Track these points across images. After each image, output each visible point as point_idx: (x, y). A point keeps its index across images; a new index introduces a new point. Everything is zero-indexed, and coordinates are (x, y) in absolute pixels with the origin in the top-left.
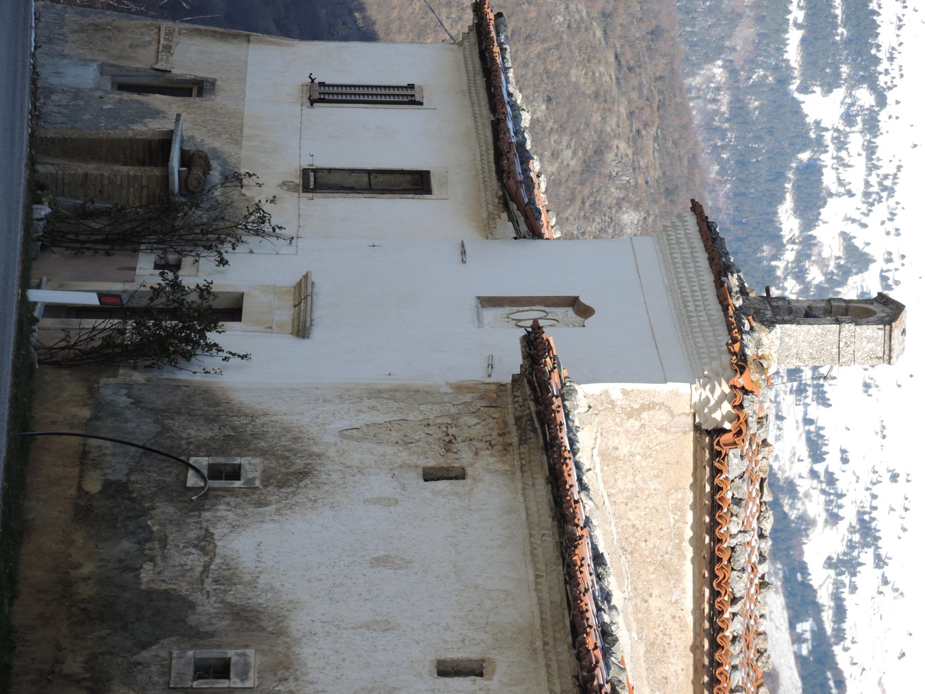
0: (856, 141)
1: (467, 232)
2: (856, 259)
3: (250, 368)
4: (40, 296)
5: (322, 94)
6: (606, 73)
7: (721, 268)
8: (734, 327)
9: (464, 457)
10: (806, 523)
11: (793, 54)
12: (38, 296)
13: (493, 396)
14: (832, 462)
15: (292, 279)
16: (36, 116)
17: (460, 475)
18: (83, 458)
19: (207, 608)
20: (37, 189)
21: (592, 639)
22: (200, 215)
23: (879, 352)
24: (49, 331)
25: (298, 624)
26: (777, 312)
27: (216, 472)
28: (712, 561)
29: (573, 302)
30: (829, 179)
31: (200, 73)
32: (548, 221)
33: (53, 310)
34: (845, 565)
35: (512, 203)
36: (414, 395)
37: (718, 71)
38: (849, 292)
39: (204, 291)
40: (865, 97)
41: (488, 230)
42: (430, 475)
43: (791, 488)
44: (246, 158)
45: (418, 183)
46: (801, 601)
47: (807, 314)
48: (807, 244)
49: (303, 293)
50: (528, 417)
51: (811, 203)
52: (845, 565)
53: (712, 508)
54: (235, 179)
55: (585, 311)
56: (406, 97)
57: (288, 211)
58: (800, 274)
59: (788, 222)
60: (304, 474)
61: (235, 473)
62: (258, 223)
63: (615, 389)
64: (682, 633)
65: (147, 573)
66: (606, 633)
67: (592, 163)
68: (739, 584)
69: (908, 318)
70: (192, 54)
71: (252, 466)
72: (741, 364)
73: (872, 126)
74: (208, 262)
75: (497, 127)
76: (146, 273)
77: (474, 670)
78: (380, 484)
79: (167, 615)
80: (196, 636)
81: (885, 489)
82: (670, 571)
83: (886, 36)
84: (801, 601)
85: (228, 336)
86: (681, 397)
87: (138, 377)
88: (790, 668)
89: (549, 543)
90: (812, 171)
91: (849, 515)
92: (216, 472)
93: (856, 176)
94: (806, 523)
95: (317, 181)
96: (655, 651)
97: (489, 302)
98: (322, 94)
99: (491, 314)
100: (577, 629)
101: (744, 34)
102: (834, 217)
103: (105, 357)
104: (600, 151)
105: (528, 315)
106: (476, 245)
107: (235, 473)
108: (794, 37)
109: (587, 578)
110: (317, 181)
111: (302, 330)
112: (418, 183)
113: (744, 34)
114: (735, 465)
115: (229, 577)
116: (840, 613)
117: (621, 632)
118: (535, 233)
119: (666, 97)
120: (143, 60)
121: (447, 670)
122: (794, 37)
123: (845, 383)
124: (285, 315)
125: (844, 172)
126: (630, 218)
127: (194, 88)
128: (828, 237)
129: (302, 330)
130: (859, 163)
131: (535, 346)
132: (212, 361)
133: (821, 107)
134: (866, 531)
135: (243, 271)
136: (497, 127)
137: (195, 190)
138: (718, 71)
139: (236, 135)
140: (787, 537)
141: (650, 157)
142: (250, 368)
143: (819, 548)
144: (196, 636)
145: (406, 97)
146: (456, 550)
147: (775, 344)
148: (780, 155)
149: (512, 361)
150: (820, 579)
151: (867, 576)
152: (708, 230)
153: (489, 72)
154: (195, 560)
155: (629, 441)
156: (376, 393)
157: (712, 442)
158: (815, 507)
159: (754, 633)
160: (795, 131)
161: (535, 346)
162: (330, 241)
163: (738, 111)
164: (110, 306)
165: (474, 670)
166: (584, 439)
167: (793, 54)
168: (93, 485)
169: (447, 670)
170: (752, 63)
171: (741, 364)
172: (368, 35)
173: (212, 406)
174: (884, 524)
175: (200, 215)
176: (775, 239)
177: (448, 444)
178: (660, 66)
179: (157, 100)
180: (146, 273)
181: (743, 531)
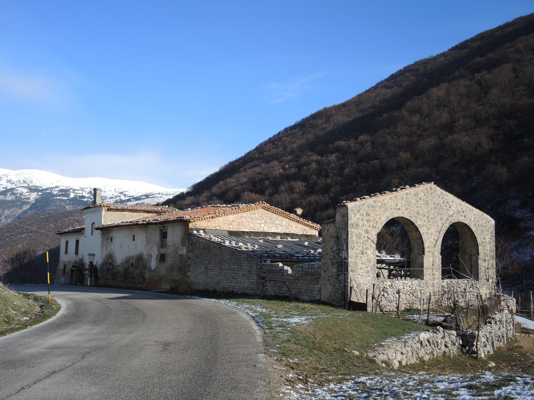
0: (76, 192)
1: (84, 236)
2: (90, 192)
3: (98, 260)
4: (89, 284)
5: (66, 252)
6: (67, 219)
7: (89, 208)
8: (96, 207)
9: (110, 237)
10: (120, 199)
11: (66, 198)
12: (89, 284)
13: (103, 234)
14: (113, 196)
15: (88, 256)
16: (68, 284)
17: (112, 238)
18: (108, 279)
19: (126, 266)
20: (76, 284)
21: (131, 224)
22: (80, 266)
23: (97, 192)
24: (93, 283)
25: (128, 256)
26: (94, 202)
27: (110, 265)
28: (123, 210)
29: (92, 224)
30: (80, 195)
31: (63, 265)
32: (83, 227)
33: (90, 283)
34: (125, 195)
35: (81, 231)
36: (102, 243)
37: (67, 207)
38: (93, 193)
39: (89, 266)
40: (71, 191)
41: (83, 234)
42: (112, 241)
43: (116, 201)
44: (73, 261)
45: (77, 242)
46: (129, 200)
47: (95, 198)
48: (88, 198)
49: (90, 255)
50: (106, 230)
51: (83, 197)
52: (125, 195)
53: (117, 210)
54: (76, 262)
55: (94, 223)
56: (67, 243)
57: (80, 256)
58: (92, 199)
59: (86, 199)
60: (111, 255)
61: (110, 263)
62: (81, 260)
63: (103, 220)
64: (135, 214)
65: (121, 272)
66: (130, 222)
67: (77, 221)
68: (126, 207)
69: (96, 187)
70: (61, 266)
71: (110, 261)
72: (100, 206)
73: (75, 190)
74: (86, 265)
75: (71, 232)
76: (87, 272)
77: (134, 237)
78: (112, 247)
79: (126, 270)
80: (129, 267)
81: (117, 190)
82: (124, 215)
83: (64, 188)
84: (129, 200)
85: (94, 263)
86: (104, 212)
87: (99, 273)
88: (352, 210)
89: (120, 228)
90: (79, 197)
91: (119, 195)
92: (110, 265)
93: (80, 192)
94: (120, 199)
95: (77, 252)
96: (133, 217)
97: (92, 234)
98: (66, 252)
99: (93, 234)
100: (130, 225)
101: (63, 204)
102: (85, 194)
103: (96, 277)
104: (75, 220)
105: (94, 229)
106: (85, 235)
107: (110, 263)
108: (64, 198)
109: (124, 224)
110: (77, 252)
111: (94, 255)
112: (77, 242)
113: (63, 204)
114: (112, 207)
115: (122, 263)
116: (131, 196)
117: (130, 220)
118: (84, 228)
119: (70, 212)
120: (61, 272)
121: (134, 240)
122: (64, 198)
123: (103, 194)
124: (92, 257)
125: (80, 193)
126: (84, 217)
127: (65, 266)
128: (87, 195)
129: (94, 255)
130: (79, 191)
131: (97, 229)
132: (97, 265)
133: (72, 195)
134: (121, 193)
135: (87, 261)
136: (71, 232)
137: (77, 267)
138: (67, 207)
139: (70, 262)
140: (122, 202)
141: (77, 214)
142: (98, 260)
143: (123, 198)
144: (129, 267)
145: (67, 243)
146: (118, 237)
147: (98, 202)
148: (78, 200)
149: (99, 231)
150: (126, 198)
151: (126, 193)
152: (84, 209)
153: (65, 233)
154: (120, 267)
155: (108, 219)
156: (102, 247)
157: (109, 209)
158: (119, 198)
159: (131, 206)
160: (75, 198)
161: (97, 229)
162: (84, 252)
163: (71, 205)
164: (90, 276)
165: (134, 237)
166: (108, 224)
167: (66, 198)
168: (111, 278)
169: (134, 240)
170: (66, 203)
171: (100, 206)
172: (60, 246)
173: (103, 265)
174: (121, 191)
175: (80, 266)
176: (87, 201)
177: (108, 239)
178: (66, 213)
179: (66, 271)
180: (87, 272)
181: (120, 206)
